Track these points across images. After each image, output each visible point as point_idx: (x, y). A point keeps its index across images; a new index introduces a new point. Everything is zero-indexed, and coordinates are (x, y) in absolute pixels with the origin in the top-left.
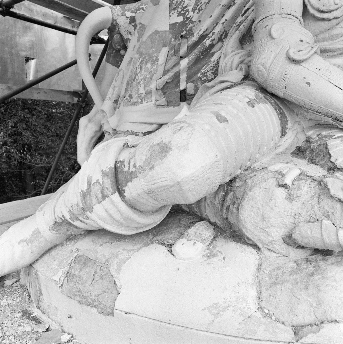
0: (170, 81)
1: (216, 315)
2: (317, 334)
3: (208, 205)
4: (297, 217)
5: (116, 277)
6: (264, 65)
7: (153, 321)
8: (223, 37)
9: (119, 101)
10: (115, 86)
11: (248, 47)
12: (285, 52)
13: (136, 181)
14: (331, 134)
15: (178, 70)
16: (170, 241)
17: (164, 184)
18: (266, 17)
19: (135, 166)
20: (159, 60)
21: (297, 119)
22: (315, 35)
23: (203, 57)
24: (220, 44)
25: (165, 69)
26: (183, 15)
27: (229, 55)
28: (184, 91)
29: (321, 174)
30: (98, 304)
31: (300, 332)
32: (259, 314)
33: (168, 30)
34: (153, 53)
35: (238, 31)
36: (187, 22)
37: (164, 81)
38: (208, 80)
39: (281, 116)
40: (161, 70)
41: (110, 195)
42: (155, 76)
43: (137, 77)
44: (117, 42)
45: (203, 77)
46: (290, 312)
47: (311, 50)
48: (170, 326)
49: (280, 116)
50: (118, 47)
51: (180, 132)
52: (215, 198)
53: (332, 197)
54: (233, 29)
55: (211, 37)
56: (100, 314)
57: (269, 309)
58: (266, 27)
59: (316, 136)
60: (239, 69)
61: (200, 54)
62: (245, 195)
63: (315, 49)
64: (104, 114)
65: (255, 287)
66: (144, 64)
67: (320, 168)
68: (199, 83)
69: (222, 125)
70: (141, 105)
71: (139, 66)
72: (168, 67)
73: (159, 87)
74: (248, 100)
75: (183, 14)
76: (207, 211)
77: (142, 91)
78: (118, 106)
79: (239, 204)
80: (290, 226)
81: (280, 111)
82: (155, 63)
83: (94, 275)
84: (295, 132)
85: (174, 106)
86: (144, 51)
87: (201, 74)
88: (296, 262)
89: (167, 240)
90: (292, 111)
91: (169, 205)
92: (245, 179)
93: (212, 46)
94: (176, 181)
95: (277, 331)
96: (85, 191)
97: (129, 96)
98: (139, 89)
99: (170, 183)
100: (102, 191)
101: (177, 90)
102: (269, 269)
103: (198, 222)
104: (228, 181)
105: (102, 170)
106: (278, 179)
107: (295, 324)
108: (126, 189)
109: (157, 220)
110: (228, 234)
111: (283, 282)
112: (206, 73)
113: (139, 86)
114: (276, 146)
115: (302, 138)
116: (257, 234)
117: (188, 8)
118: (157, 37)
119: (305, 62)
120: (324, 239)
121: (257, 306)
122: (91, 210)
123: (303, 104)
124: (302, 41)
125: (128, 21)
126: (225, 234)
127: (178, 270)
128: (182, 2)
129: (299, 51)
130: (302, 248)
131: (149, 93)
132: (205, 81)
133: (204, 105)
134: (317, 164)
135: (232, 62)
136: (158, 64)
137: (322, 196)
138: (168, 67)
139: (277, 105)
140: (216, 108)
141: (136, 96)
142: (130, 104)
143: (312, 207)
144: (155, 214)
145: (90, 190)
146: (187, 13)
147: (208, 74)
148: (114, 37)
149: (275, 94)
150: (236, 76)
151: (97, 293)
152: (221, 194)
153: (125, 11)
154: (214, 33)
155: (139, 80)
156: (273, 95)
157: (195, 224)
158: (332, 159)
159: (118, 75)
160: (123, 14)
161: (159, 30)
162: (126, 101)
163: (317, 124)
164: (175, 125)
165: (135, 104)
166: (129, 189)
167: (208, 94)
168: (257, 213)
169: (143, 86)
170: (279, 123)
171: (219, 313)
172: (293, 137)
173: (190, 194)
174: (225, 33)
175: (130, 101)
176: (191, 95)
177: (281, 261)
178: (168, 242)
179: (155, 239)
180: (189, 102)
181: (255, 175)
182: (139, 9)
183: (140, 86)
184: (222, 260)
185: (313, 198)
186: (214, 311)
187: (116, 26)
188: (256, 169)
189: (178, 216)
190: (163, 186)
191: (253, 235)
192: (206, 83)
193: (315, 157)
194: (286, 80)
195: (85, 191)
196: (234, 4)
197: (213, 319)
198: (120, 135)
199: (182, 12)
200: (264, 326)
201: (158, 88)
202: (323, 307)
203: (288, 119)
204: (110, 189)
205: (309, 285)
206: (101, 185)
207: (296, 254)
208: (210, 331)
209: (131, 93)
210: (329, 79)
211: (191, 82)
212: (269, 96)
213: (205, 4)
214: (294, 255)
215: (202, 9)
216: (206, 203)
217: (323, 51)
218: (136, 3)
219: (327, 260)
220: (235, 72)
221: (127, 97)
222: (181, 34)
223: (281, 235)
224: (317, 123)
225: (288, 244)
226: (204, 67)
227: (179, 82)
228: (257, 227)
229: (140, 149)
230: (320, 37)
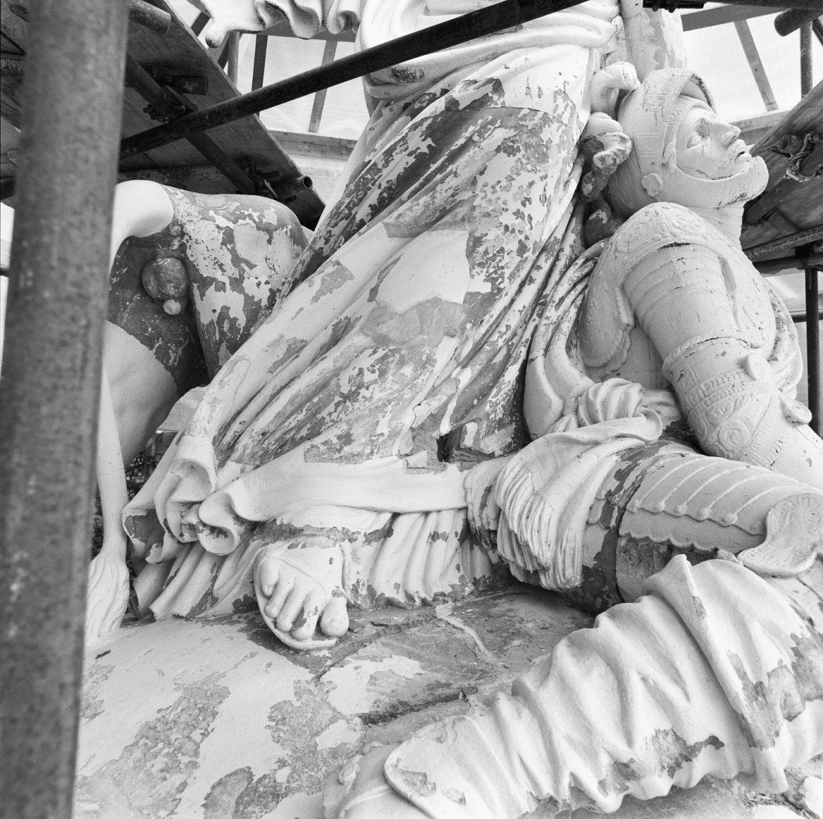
6: (747, 422)
10: (215, 399)
20: (435, 363)
33: (462, 303)
34: (423, 345)
66: (392, 366)
70: (367, 463)
75: (493, 278)
82: (424, 367)
85: (437, 471)
86: (393, 335)
87: (491, 407)
97: (339, 437)
98: (378, 422)
101: (436, 435)
113: (380, 415)
117: (505, 270)
118: (436, 312)
125: (220, 236)
131: (394, 434)
136: (432, 371)
141: (363, 440)
142: (337, 455)
146: (500, 280)
159: (231, 371)
161: (444, 297)
162: (323, 448)
165: (353, 458)
169: (389, 416)
175: (339, 451)
183: (383, 417)
209: (350, 429)
211: (473, 421)
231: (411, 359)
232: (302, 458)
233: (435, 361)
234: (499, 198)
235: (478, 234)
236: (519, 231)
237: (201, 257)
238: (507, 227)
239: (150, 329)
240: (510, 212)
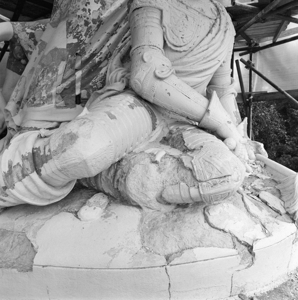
0: (67, 87)
1: (113, 256)
2: (180, 257)
3: (103, 179)
4: (164, 182)
5: (33, 240)
6: (139, 80)
7: (65, 269)
8: (108, 56)
9: (22, 103)
11: (127, 65)
12: (153, 71)
13: (50, 162)
14: (184, 128)
15: (74, 80)
16: (75, 209)
17: (73, 162)
18: (140, 47)
19: (49, 151)
21: (163, 118)
22: (172, 61)
23: (93, 71)
24: (106, 61)
25: (64, 78)
26: (78, 38)
27: (114, 71)
28: (79, 96)
29: (178, 154)
30: (17, 265)
31: (170, 258)
32: (143, 251)
34: (54, 65)
35: (119, 53)
36: (81, 44)
37: (63, 87)
38: (97, 88)
39: (152, 116)
40: (60, 79)
41: (29, 174)
42: (55, 84)
43: (39, 84)
44: (18, 52)
45: (93, 86)
46: (163, 247)
47: (170, 71)
48: (80, 269)
49: (151, 116)
50: (19, 57)
51: (84, 125)
52: (108, 174)
53: (185, 168)
54: (116, 51)
55: (100, 56)
56: (20, 272)
57: (150, 247)
58: (139, 53)
59: (176, 129)
60: (121, 81)
61: (91, 68)
62: (130, 170)
63: (172, 71)
64: (8, 113)
65: (139, 233)
66: (45, 74)
67: (270, 289)
68: (90, 90)
69: (112, 121)
70: (43, 107)
71: (41, 74)
72: (66, 76)
73: (58, 92)
74: (129, 104)
76: (103, 185)
77: (44, 94)
78: (21, 107)
79: (126, 177)
80: (160, 190)
81: (151, 112)
82: (55, 73)
83: (12, 243)
84: (162, 127)
85: (71, 108)
86: (45, 63)
87: (92, 84)
88: (165, 214)
89: (73, 209)
90: (159, 112)
91: (74, 180)
92: (129, 160)
93: (100, 62)
94: (82, 159)
95: (155, 259)
96: (6, 172)
97: (33, 99)
98: (41, 93)
99: (78, 161)
100: (22, 172)
102: (148, 221)
103: (95, 194)
104: (117, 161)
105: (22, 155)
106: (151, 158)
107: (166, 254)
108: (42, 169)
109: (65, 193)
110: (118, 200)
111: (158, 228)
112: (96, 82)
113: (42, 91)
114: (150, 137)
115: (167, 131)
116: (139, 197)
117: (82, 33)
118: (56, 53)
119: (166, 79)
120: (182, 195)
121: (141, 245)
122: (13, 186)
123: (166, 108)
124: (163, 65)
126: (116, 201)
127: (83, 228)
128: (77, 28)
129: (162, 72)
130: (169, 204)
132: (95, 89)
133: (99, 107)
134: (176, 148)
135: (116, 76)
136: (57, 74)
137: (179, 168)
138: (66, 76)
139: (149, 108)
140: (107, 109)
141: (39, 99)
142: (33, 105)
143: (174, 175)
144: (64, 188)
145: (12, 171)
146: (81, 37)
147: (98, 83)
148: (16, 48)
149: (147, 100)
150: (119, 86)
151: (16, 257)
152: (112, 171)
153: (26, 27)
154: (101, 53)
155: (41, 86)
156: (146, 101)
157: (93, 196)
158: (185, 144)
159: (21, 81)
160: (24, 30)
161: (58, 47)
162: (30, 103)
163: (176, 121)
164: (79, 120)
166: (45, 169)
167: (99, 99)
168: (138, 182)
169: (45, 91)
170: (151, 121)
171: (115, 254)
172: (161, 131)
173: (92, 169)
174: (110, 53)
175: (33, 103)
176: (85, 99)
177: (156, 214)
178: (74, 210)
179: (63, 209)
180: (83, 105)
181: (136, 157)
182: (38, 27)
183: (43, 91)
184: (116, 218)
185: (174, 169)
186: (112, 253)
187: (17, 39)
188: (136, 152)
189: (79, 191)
190: (73, 164)
191: (136, 198)
192: (96, 90)
193: (175, 143)
194: (155, 91)
195: (6, 172)
196: (116, 33)
197: (111, 259)
198: (25, 131)
199: (77, 36)
200: (147, 258)
201: (57, 93)
202: (183, 240)
203: (157, 117)
204: (30, 169)
205: (174, 227)
206: (21, 167)
207: (165, 209)
208: (110, 268)
209: (34, 96)
210: (182, 91)
212: (143, 102)
213: (94, 31)
214: (164, 209)
215: (92, 35)
216: (102, 179)
217: (177, 72)
218: (35, 22)
219: (185, 211)
220: (118, 83)
221: (31, 99)
222: (76, 52)
223: (155, 196)
224: (176, 120)
225: (159, 202)
226: (94, 78)
227: (75, 89)
228: (139, 191)
229: (53, 138)
230: (175, 62)
231: (50, 71)
232: (26, 106)
233: (58, 70)
234: (76, 5)
235: (69, 21)
236: (84, 17)
237: (24, 44)
238: (79, 16)
239: (20, 70)
240: (81, 10)
